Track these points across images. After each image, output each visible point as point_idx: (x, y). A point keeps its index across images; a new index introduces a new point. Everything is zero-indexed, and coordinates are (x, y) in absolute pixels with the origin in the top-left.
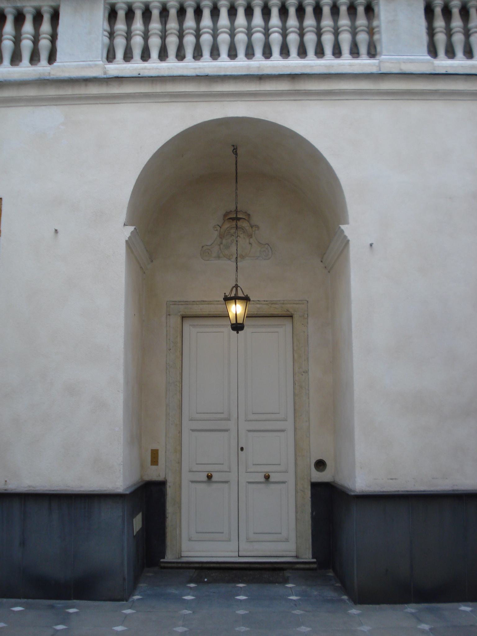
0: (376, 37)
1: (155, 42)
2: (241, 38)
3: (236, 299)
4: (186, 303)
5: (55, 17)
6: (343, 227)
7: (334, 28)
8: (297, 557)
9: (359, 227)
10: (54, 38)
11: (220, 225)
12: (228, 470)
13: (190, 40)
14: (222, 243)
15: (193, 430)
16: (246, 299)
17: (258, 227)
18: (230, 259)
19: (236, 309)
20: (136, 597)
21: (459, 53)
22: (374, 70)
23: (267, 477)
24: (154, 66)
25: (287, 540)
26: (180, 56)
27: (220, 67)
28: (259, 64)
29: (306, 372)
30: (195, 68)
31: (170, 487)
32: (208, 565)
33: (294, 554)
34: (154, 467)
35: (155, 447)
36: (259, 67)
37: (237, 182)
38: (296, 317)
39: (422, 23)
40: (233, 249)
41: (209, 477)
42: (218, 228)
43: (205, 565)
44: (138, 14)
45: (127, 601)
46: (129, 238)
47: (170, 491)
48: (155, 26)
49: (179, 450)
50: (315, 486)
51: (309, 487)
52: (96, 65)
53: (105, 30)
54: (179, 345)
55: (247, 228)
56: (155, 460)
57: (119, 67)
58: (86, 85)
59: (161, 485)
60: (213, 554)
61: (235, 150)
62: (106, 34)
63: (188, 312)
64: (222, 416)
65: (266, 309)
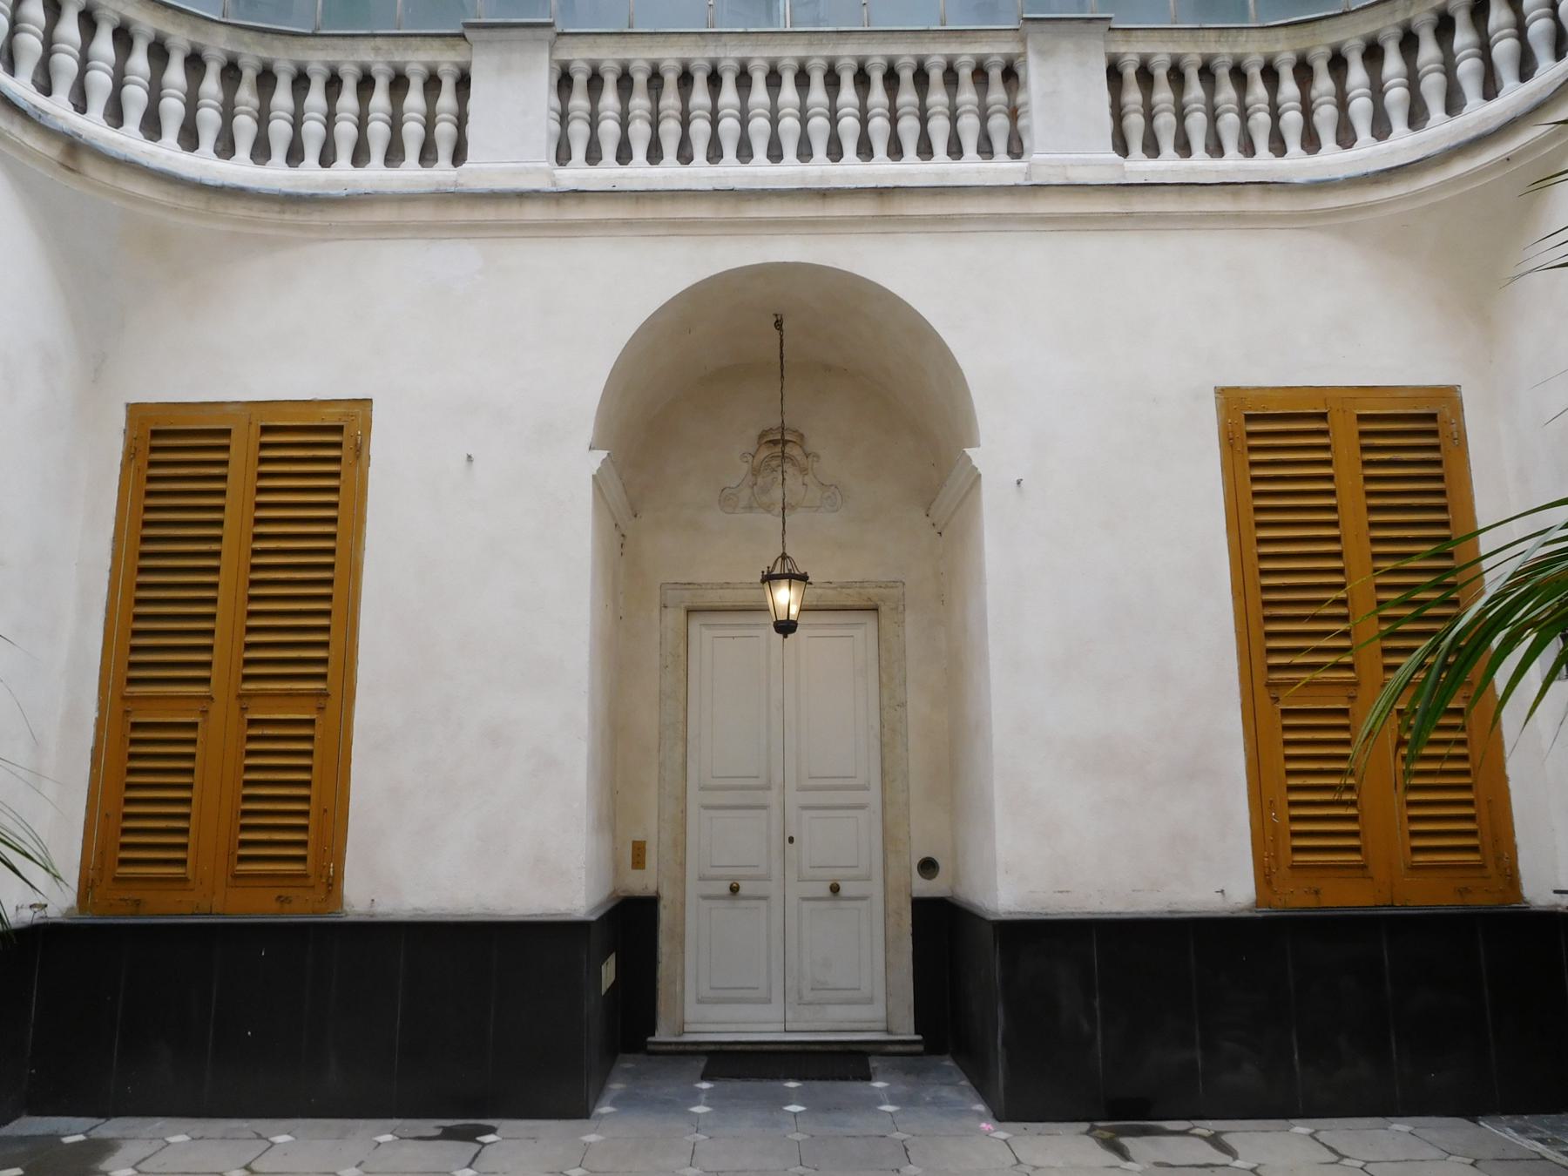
0: (1021, 123)
1: (640, 132)
2: (789, 125)
5: (463, 83)
6: (968, 451)
10: (461, 121)
13: (700, 128)
16: (803, 578)
17: (817, 456)
19: (785, 598)
25: (870, 1001)
29: (903, 705)
35: (639, 837)
38: (883, 609)
39: (1105, 97)
40: (777, 494)
47: (665, 915)
49: (680, 844)
53: (553, 109)
54: (683, 658)
56: (638, 860)
57: (577, 174)
61: (778, 324)
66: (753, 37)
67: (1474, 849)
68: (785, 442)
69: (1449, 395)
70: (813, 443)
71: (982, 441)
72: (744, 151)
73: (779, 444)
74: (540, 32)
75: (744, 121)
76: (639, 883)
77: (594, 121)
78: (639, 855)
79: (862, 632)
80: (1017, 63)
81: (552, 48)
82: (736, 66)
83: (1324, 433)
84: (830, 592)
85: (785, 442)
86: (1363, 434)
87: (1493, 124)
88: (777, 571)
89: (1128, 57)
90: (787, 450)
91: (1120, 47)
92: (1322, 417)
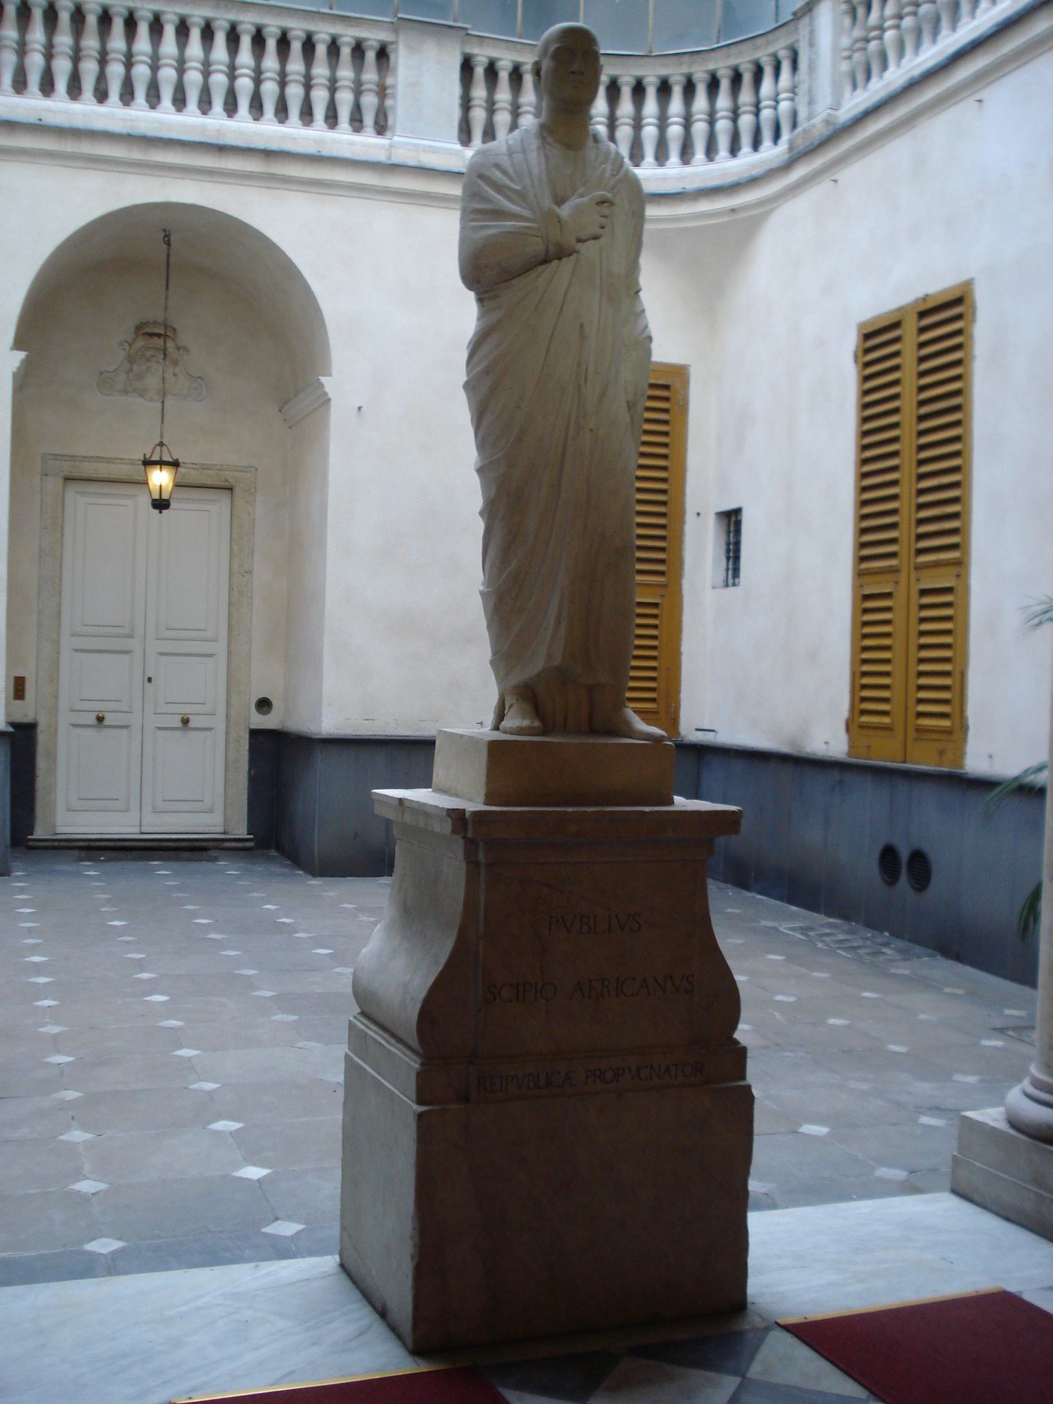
0: (388, 102)
2: (193, 77)
3: (161, 463)
4: (72, 457)
6: (323, 379)
7: (329, 80)
9: (346, 379)
11: (130, 340)
12: (127, 709)
13: (116, 70)
14: (131, 370)
16: (175, 464)
17: (186, 349)
18: (141, 396)
19: (160, 479)
22: (381, 157)
23: (185, 722)
25: (211, 811)
28: (217, 125)
29: (250, 572)
30: (124, 120)
32: (98, 844)
33: (221, 830)
37: (167, 286)
38: (237, 491)
39: (456, 90)
41: (100, 719)
42: (127, 346)
43: (93, 844)
46: (19, 369)
47: (42, 738)
49: (54, 678)
50: (255, 734)
51: (247, 736)
60: (103, 830)
63: (76, 474)
64: (120, 631)
67: (653, 700)
70: (185, 338)
71: (334, 372)
73: (156, 336)
75: (155, 67)
76: (26, 711)
79: (217, 509)
80: (390, 49)
84: (192, 472)
87: (728, 180)
88: (156, 458)
89: (479, 59)
91: (474, 50)
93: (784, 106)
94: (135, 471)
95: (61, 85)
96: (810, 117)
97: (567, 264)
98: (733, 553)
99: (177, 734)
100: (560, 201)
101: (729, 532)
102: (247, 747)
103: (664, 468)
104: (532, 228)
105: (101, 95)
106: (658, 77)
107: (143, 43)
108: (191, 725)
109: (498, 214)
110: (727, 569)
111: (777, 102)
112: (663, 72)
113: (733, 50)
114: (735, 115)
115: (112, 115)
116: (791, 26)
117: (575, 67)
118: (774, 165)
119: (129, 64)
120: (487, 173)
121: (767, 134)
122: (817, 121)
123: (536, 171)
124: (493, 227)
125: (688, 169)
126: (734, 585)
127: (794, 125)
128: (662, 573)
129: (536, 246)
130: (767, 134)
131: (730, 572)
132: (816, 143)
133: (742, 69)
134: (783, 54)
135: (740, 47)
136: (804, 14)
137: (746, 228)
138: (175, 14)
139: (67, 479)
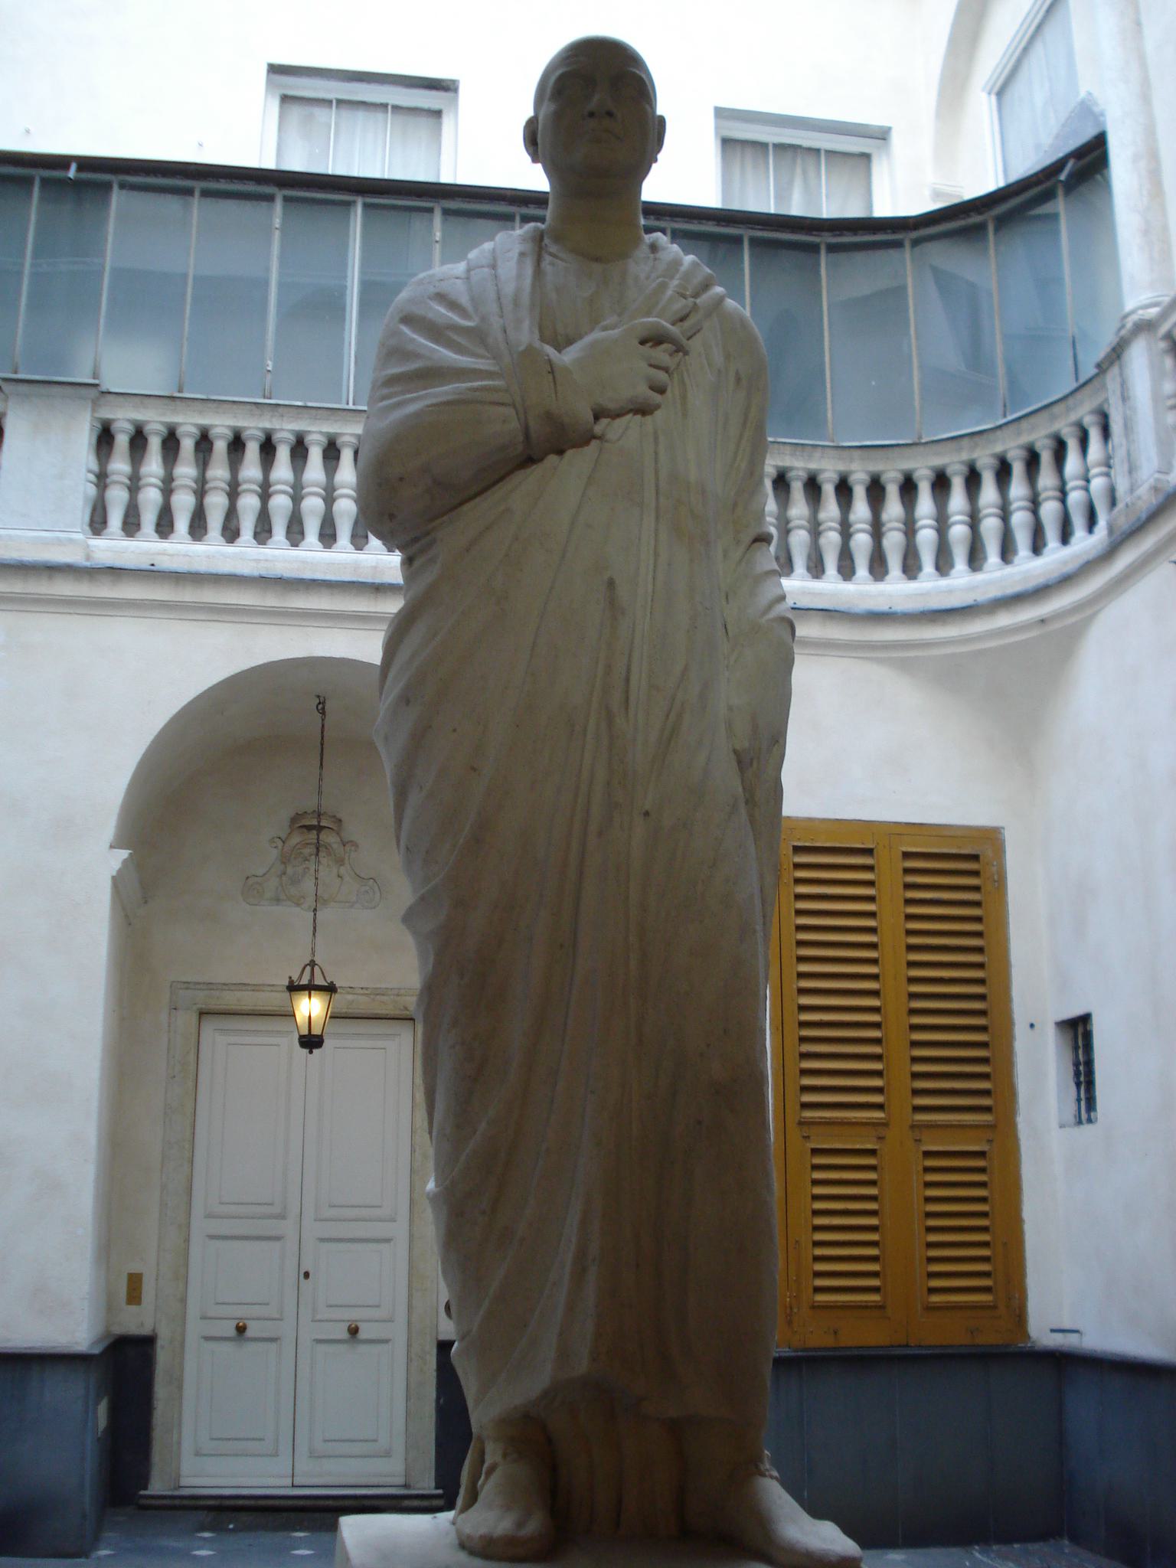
1: (183, 503)
3: (310, 988)
8: (406, 1486)
11: (283, 837)
13: (249, 503)
15: (212, 1237)
16: (330, 989)
17: (355, 845)
18: (298, 905)
19: (310, 1008)
20: (103, 1553)
21: (862, 571)
23: (354, 1331)
24: (180, 551)
25: (387, 1454)
26: (231, 533)
27: (304, 562)
30: (258, 561)
31: (163, 1347)
33: (401, 1481)
34: (133, 1308)
35: (135, 1268)
36: (375, 567)
40: (308, 885)
41: (241, 1330)
42: (280, 843)
44: (155, 444)
45: (87, 1557)
46: (119, 871)
47: (163, 1357)
48: (186, 471)
49: (182, 1274)
51: (434, 1351)
52: (71, 540)
53: (90, 471)
54: (193, 1067)
55: (335, 846)
56: (134, 1294)
57: (113, 547)
58: (50, 578)
59: (146, 1343)
62: (92, 477)
63: (213, 1005)
65: (363, 1005)
66: (313, 412)
67: (987, 1290)
68: (319, 829)
69: (992, 837)
72: (295, 532)
73: (314, 828)
74: (83, 391)
75: (297, 498)
76: (134, 1322)
77: (134, 485)
78: (134, 1288)
81: (94, 410)
82: (292, 438)
83: (870, 868)
85: (319, 829)
86: (907, 871)
87: (1030, 585)
90: (323, 836)
92: (869, 852)
93: (1097, 484)
94: (275, 999)
95: (182, 524)
96: (1132, 490)
97: (577, 463)
98: (1084, 1076)
99: (343, 1348)
100: (561, 343)
101: (1076, 1048)
102: (434, 1366)
103: (980, 966)
104: (495, 389)
105: (231, 533)
106: (933, 468)
107: (282, 470)
108: (362, 1335)
109: (431, 375)
110: (1079, 1100)
111: (1088, 481)
112: (938, 461)
113: (1024, 424)
114: (1035, 504)
115: (245, 556)
116: (1095, 382)
117: (593, 104)
118: (1090, 557)
119: (265, 494)
120: (419, 311)
121: (1078, 522)
122: (1143, 491)
123: (509, 289)
124: (412, 400)
125: (979, 577)
126: (1090, 1121)
127: (1113, 502)
128: (987, 1109)
129: (502, 426)
130: (1078, 522)
131: (1083, 1103)
132: (1144, 516)
133: (1038, 447)
134: (1091, 422)
135: (1032, 420)
136: (1112, 364)
137: (1061, 642)
138: (321, 433)
139: (202, 1014)
